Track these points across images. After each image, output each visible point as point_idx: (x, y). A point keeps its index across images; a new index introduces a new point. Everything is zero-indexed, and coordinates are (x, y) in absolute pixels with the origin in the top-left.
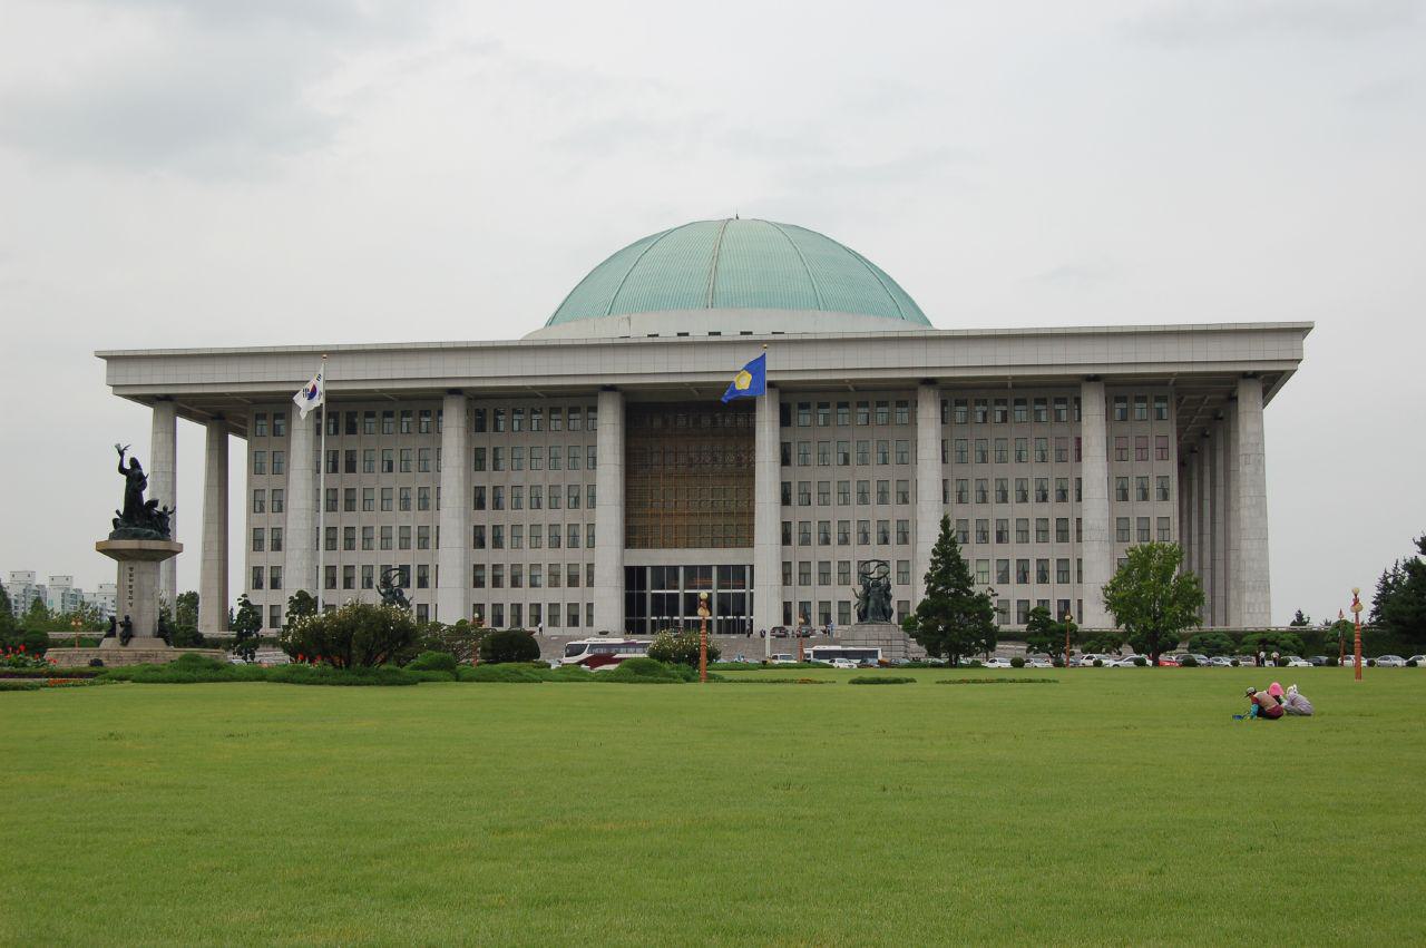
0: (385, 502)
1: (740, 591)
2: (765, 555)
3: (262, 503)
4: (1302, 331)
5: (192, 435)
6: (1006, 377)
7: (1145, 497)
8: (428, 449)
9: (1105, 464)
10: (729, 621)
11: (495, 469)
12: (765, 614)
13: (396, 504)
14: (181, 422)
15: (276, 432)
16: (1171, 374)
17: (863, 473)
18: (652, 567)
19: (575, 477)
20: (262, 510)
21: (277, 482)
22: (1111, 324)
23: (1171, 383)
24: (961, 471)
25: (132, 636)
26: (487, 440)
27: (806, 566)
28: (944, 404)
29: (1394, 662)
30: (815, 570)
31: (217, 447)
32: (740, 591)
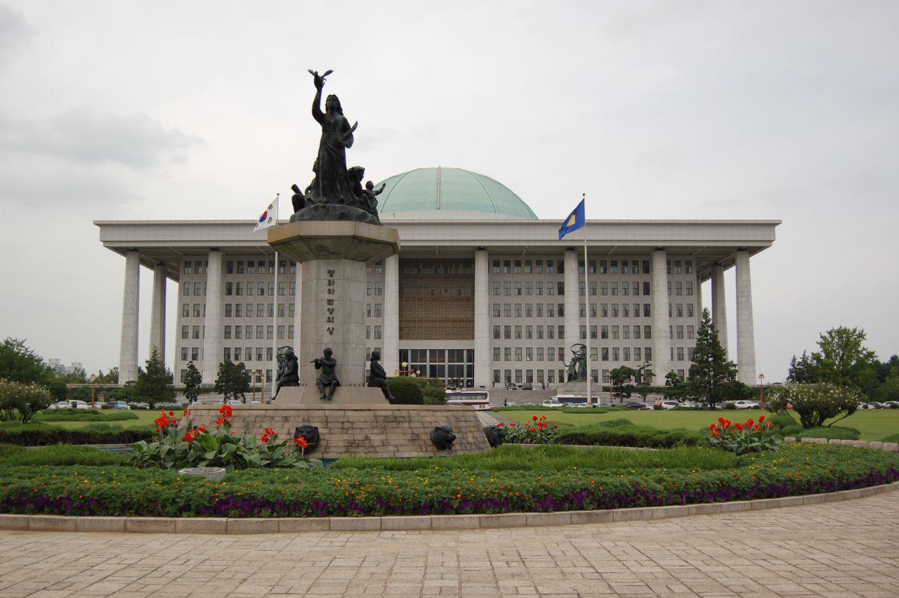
0: (259, 312)
1: (414, 364)
2: (482, 343)
3: (187, 311)
4: (772, 225)
5: (147, 275)
6: (434, 247)
7: (616, 315)
8: (285, 282)
9: (488, 296)
10: (454, 380)
11: (237, 294)
12: (482, 376)
13: (513, 313)
14: (142, 268)
15: (196, 272)
16: (524, 247)
17: (529, 299)
18: (431, 350)
19: (197, 300)
20: (188, 315)
21: (646, 300)
22: (126, 220)
23: (524, 253)
24: (679, 300)
25: (338, 384)
26: (233, 278)
27: (540, 353)
28: (668, 263)
29: (748, 405)
30: (502, 352)
31: (160, 281)
32: (414, 364)
